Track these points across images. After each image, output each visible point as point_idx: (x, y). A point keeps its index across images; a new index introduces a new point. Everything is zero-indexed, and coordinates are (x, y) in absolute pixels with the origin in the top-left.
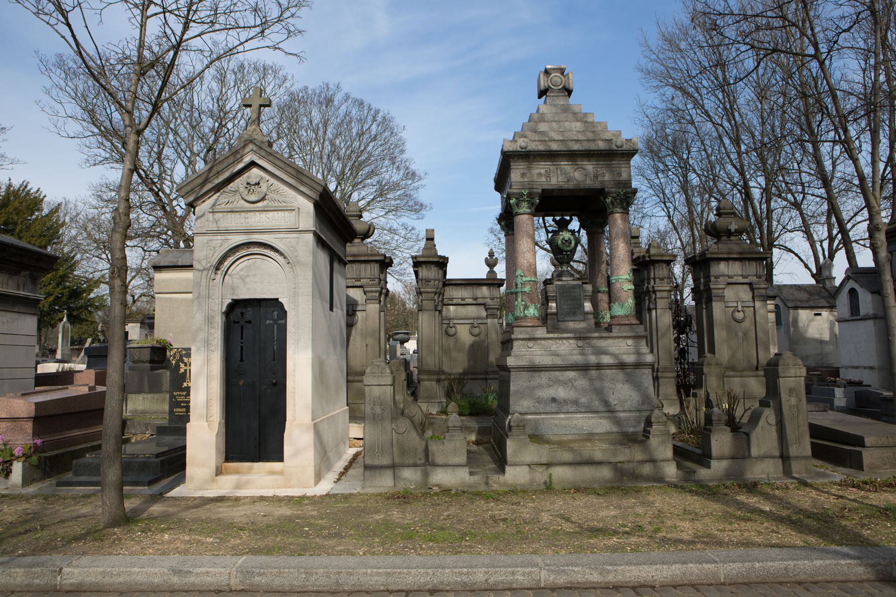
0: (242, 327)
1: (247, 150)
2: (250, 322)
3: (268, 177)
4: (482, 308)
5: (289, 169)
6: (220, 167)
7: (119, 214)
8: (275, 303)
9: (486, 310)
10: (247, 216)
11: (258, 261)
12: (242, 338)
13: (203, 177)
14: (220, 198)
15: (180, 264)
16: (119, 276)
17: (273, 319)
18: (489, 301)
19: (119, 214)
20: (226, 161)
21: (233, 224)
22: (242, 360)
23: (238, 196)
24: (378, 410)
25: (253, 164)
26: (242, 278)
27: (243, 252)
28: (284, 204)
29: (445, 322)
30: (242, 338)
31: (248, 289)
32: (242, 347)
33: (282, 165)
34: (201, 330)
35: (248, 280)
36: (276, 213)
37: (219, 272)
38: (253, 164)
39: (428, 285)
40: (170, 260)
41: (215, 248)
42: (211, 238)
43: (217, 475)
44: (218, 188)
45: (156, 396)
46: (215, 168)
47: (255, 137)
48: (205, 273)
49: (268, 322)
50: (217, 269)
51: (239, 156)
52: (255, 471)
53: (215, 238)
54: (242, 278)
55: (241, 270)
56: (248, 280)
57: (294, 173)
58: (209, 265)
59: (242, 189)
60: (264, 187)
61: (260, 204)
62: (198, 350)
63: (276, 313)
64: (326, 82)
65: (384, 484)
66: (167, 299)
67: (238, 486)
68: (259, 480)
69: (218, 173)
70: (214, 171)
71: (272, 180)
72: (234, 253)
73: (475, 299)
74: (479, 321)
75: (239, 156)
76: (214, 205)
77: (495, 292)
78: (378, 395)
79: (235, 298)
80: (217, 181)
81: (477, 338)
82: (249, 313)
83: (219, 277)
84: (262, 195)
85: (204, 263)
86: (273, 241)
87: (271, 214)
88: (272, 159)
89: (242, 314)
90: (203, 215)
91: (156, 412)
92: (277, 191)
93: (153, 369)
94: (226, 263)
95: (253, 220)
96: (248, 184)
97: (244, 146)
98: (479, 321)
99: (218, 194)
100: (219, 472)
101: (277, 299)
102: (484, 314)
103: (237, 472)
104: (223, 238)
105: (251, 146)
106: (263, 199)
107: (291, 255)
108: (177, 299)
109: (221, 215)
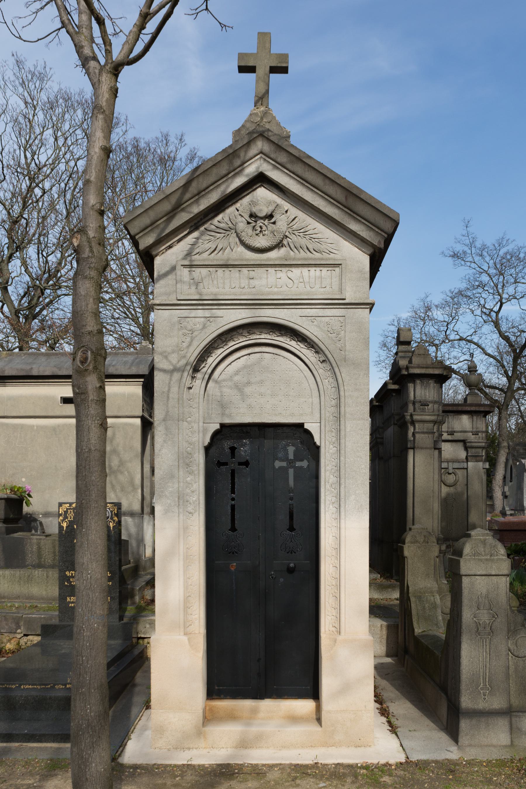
0: (233, 473)
1: (253, 150)
2: (246, 464)
3: (286, 205)
4: (460, 446)
5: (331, 190)
6: (204, 182)
7: (89, 241)
8: (297, 432)
9: (466, 449)
10: (252, 274)
11: (267, 356)
12: (233, 492)
13: (173, 200)
14: (203, 243)
15: (35, 373)
16: (95, 368)
17: (286, 459)
18: (471, 437)
19: (89, 241)
20: (215, 170)
21: (227, 289)
22: (233, 529)
23: (233, 238)
24: (485, 617)
25: (261, 179)
26: (239, 388)
27: (241, 341)
28: (317, 255)
29: (444, 465)
30: (233, 492)
31: (250, 407)
32: (233, 507)
33: (318, 181)
34: (172, 477)
35: (248, 390)
36: (305, 270)
37: (199, 375)
38: (261, 179)
39: (423, 410)
40: (20, 367)
41: (192, 331)
42: (185, 313)
43: (204, 725)
44: (196, 223)
45: (18, 572)
46: (194, 184)
47: (267, 126)
48: (176, 376)
49: (278, 464)
50: (196, 369)
51: (238, 162)
52: (261, 715)
53: (193, 313)
54: (239, 388)
55: (237, 373)
56: (248, 390)
57: (339, 194)
58: (183, 362)
59: (241, 225)
60: (282, 222)
61: (273, 255)
62: (166, 511)
63: (291, 450)
64: (165, 132)
65: (495, 742)
66: (15, 426)
67: (244, 744)
68: (274, 731)
69: (200, 194)
70: (193, 188)
71: (294, 211)
72: (226, 342)
73: (451, 433)
74: (456, 465)
75: (238, 162)
76: (189, 254)
77: (480, 424)
78: (484, 591)
79: (227, 421)
80: (196, 209)
81: (452, 489)
82: (245, 449)
83: (198, 384)
84: (279, 237)
85: (174, 358)
86: (299, 321)
87: (296, 272)
88: (299, 168)
89: (233, 449)
90: (173, 269)
91: (18, 597)
92: (303, 232)
93: (9, 531)
94: (210, 360)
95: (264, 282)
96: (251, 216)
97: (248, 144)
98: (456, 465)
99: (196, 234)
100: (209, 718)
101: (301, 425)
102: (463, 454)
103: (232, 717)
104: (207, 313)
105: (260, 145)
106: (279, 245)
107: (331, 348)
108: (32, 427)
109: (204, 271)
